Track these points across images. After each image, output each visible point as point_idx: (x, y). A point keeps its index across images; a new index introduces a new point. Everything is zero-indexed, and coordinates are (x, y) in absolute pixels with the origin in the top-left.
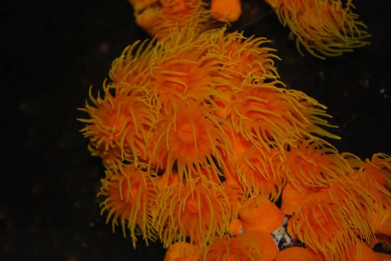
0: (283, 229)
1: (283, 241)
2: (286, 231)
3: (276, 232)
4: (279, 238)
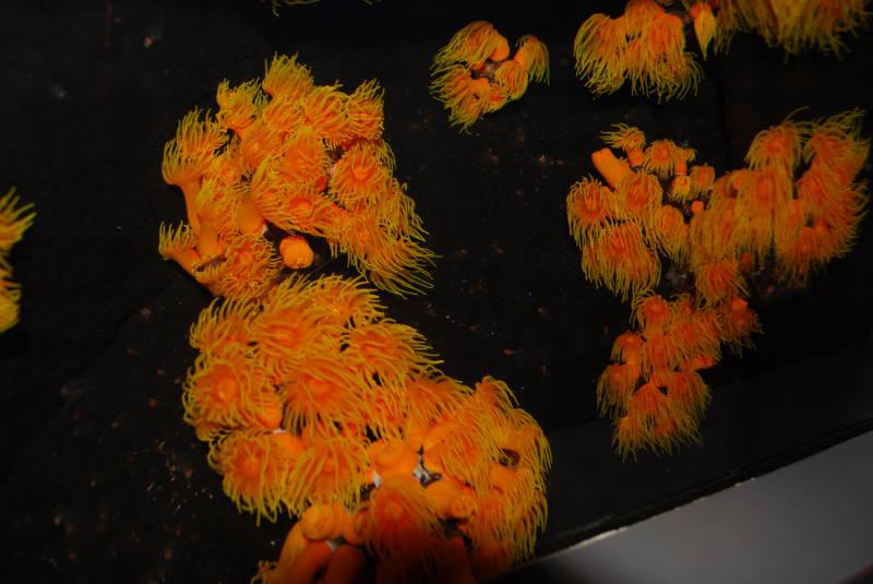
0: (420, 466)
1: (423, 478)
3: (415, 471)
4: (419, 475)
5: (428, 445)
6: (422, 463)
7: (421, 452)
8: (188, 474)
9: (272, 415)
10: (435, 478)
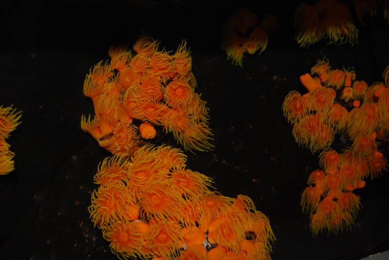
1: (207, 246)
2: (208, 241)
3: (204, 243)
4: (206, 245)
5: (211, 229)
6: (207, 239)
7: (207, 233)
8: (94, 239)
9: (134, 211)
10: (213, 246)
